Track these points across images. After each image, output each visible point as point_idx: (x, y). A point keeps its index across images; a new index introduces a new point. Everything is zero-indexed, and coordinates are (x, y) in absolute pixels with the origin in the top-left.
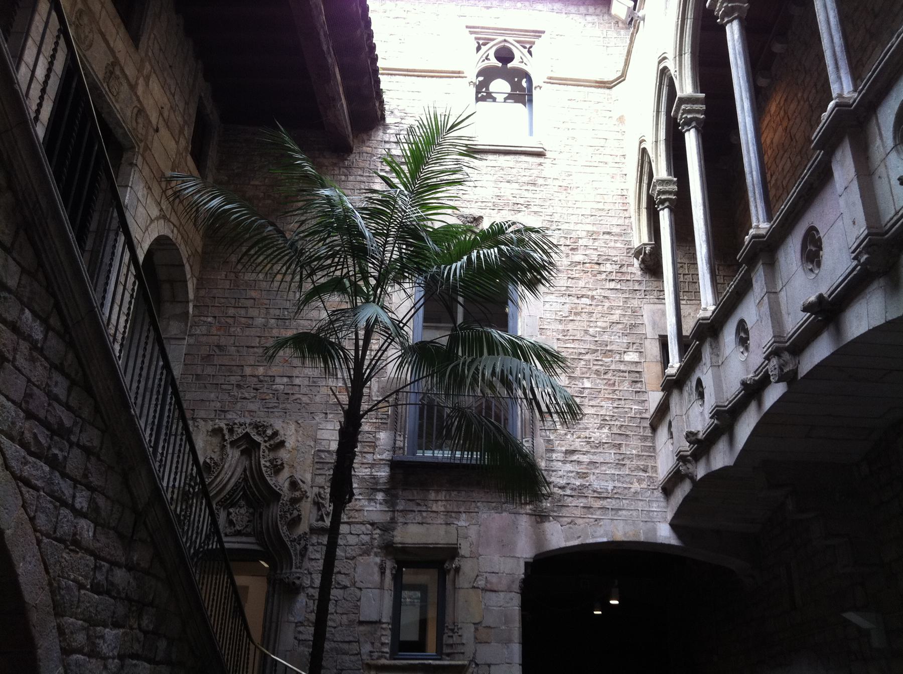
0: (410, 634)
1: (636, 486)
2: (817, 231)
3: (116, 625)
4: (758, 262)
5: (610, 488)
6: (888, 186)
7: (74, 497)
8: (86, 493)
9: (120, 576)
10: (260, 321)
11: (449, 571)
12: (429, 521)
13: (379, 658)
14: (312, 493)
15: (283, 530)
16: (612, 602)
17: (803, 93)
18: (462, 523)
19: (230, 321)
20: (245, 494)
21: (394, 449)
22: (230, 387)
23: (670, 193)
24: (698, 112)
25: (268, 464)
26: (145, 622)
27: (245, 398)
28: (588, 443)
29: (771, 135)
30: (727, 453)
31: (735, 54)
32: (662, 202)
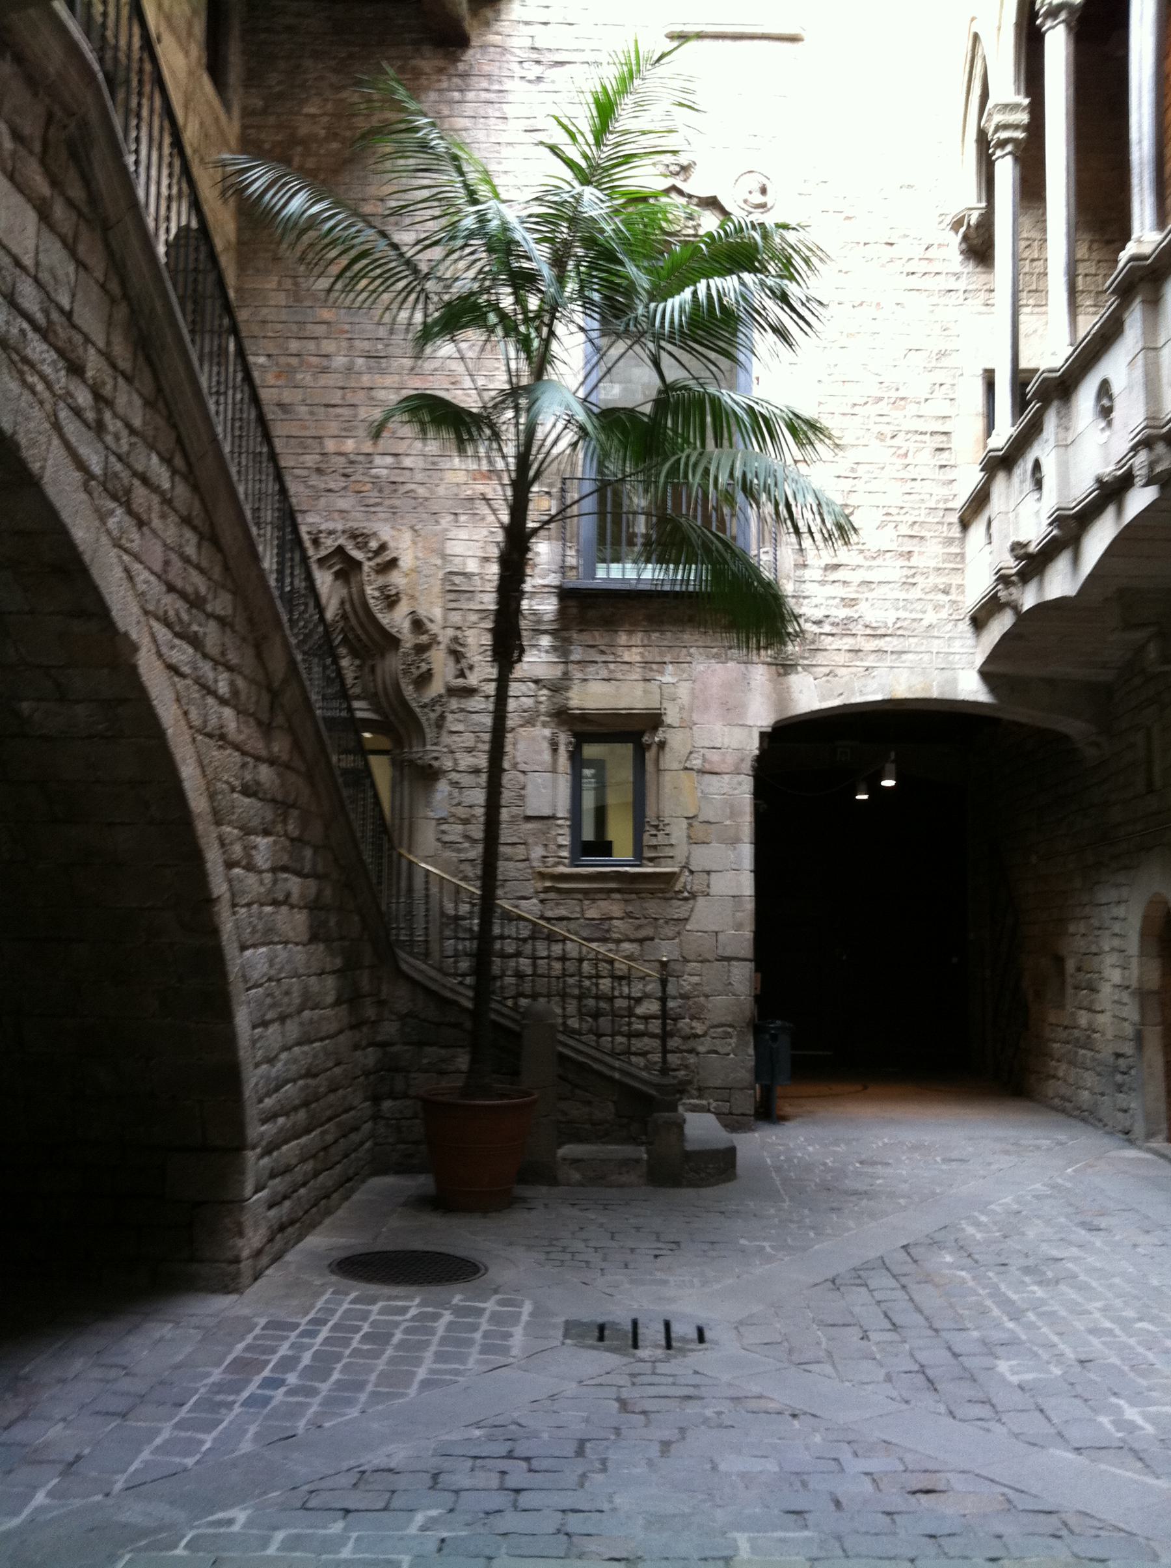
0: (588, 834)
1: (930, 617)
3: (266, 833)
7: (216, 681)
8: (226, 675)
9: (265, 773)
10: (340, 361)
11: (649, 746)
12: (619, 676)
13: (557, 864)
14: (445, 636)
15: (408, 691)
18: (667, 679)
19: (294, 361)
20: (345, 637)
21: (563, 569)
22: (304, 473)
23: (1016, 127)
25: (377, 594)
26: (290, 827)
27: (330, 491)
30: (1069, 576)
32: (1002, 144)
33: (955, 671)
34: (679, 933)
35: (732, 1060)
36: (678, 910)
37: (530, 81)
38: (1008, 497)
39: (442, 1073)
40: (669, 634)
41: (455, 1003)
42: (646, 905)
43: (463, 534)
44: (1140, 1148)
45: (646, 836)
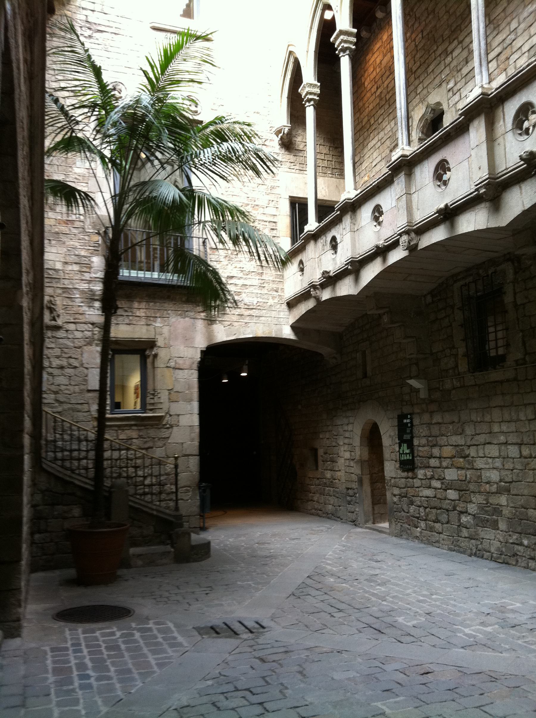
1: (271, 302)
2: (448, 163)
4: (401, 172)
5: (255, 303)
6: (503, 152)
11: (149, 356)
16: (243, 374)
17: (412, 34)
18: (158, 325)
23: (315, 94)
24: (351, 42)
28: (242, 271)
29: (380, 57)
31: (396, 17)
32: (309, 100)
33: (280, 325)
34: (165, 444)
35: (190, 503)
36: (164, 433)
37: (85, 37)
38: (315, 252)
39: (65, 518)
40: (158, 304)
41: (72, 483)
42: (149, 431)
43: (54, 250)
44: (361, 527)
45: (148, 399)
